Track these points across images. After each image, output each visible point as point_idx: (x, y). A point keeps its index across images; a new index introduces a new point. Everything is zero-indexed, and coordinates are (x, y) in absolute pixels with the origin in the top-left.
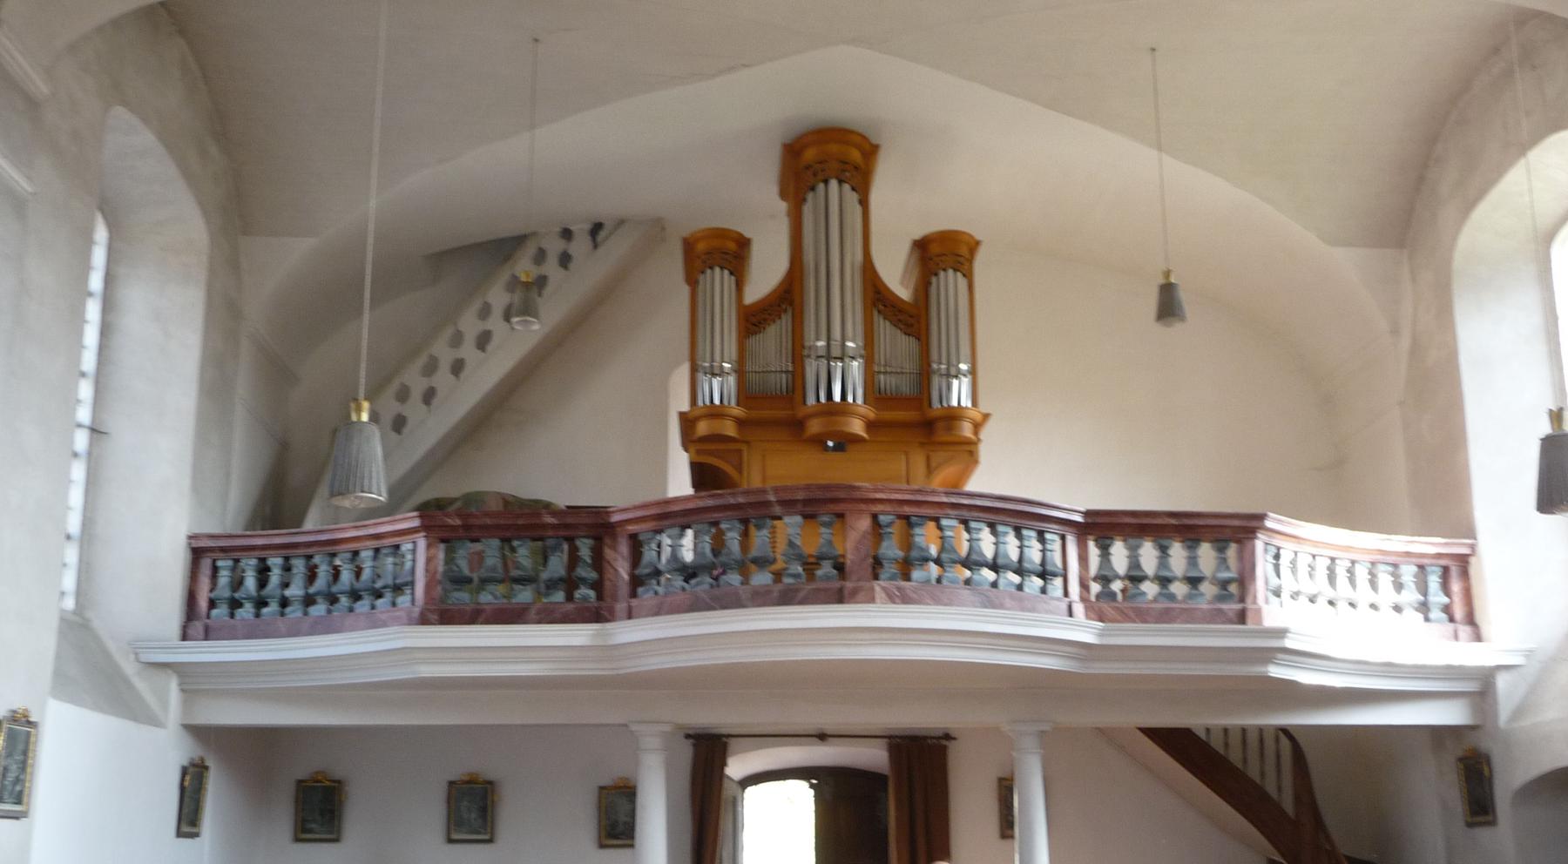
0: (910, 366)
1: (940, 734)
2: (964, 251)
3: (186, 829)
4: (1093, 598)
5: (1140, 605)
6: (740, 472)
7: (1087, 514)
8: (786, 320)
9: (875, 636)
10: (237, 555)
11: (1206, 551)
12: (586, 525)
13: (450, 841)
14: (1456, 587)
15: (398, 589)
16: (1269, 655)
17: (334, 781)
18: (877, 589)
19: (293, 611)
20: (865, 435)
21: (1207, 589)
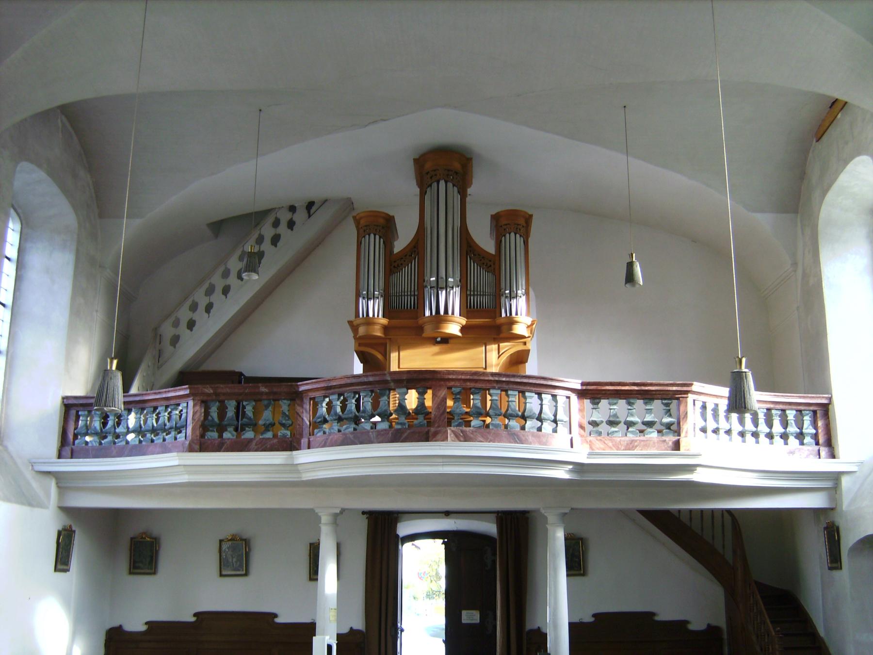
3: (60, 567)
8: (414, 264)
9: (445, 460)
13: (221, 575)
14: (820, 423)
15: (179, 430)
17: (153, 538)
18: (449, 431)
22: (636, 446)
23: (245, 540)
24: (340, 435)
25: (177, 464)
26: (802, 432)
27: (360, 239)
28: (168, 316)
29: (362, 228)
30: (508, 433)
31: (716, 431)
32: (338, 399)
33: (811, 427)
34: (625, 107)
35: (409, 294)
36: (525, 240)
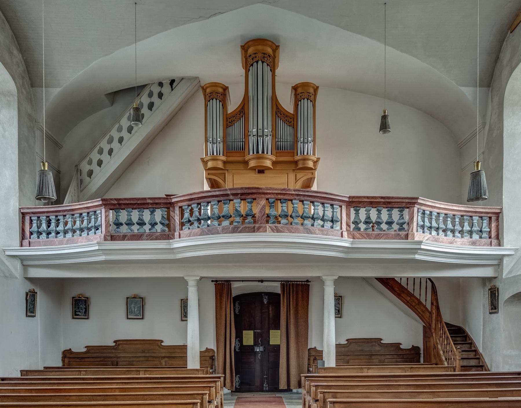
0: (290, 138)
1: (305, 280)
2: (312, 90)
3: (29, 314)
4: (352, 230)
5: (368, 232)
6: (225, 182)
7: (350, 197)
8: (242, 120)
10: (38, 215)
11: (396, 213)
12: (163, 203)
13: (128, 318)
14: (493, 225)
16: (415, 251)
17: (86, 298)
19: (60, 236)
20: (272, 167)
21: (395, 227)
22: (382, 237)
23: (142, 298)
24: (198, 229)
25: (98, 249)
26: (481, 230)
27: (207, 103)
28: (84, 158)
29: (207, 95)
30: (304, 228)
31: (430, 228)
32: (197, 207)
33: (487, 228)
34: (385, 3)
35: (239, 140)
36: (314, 104)
